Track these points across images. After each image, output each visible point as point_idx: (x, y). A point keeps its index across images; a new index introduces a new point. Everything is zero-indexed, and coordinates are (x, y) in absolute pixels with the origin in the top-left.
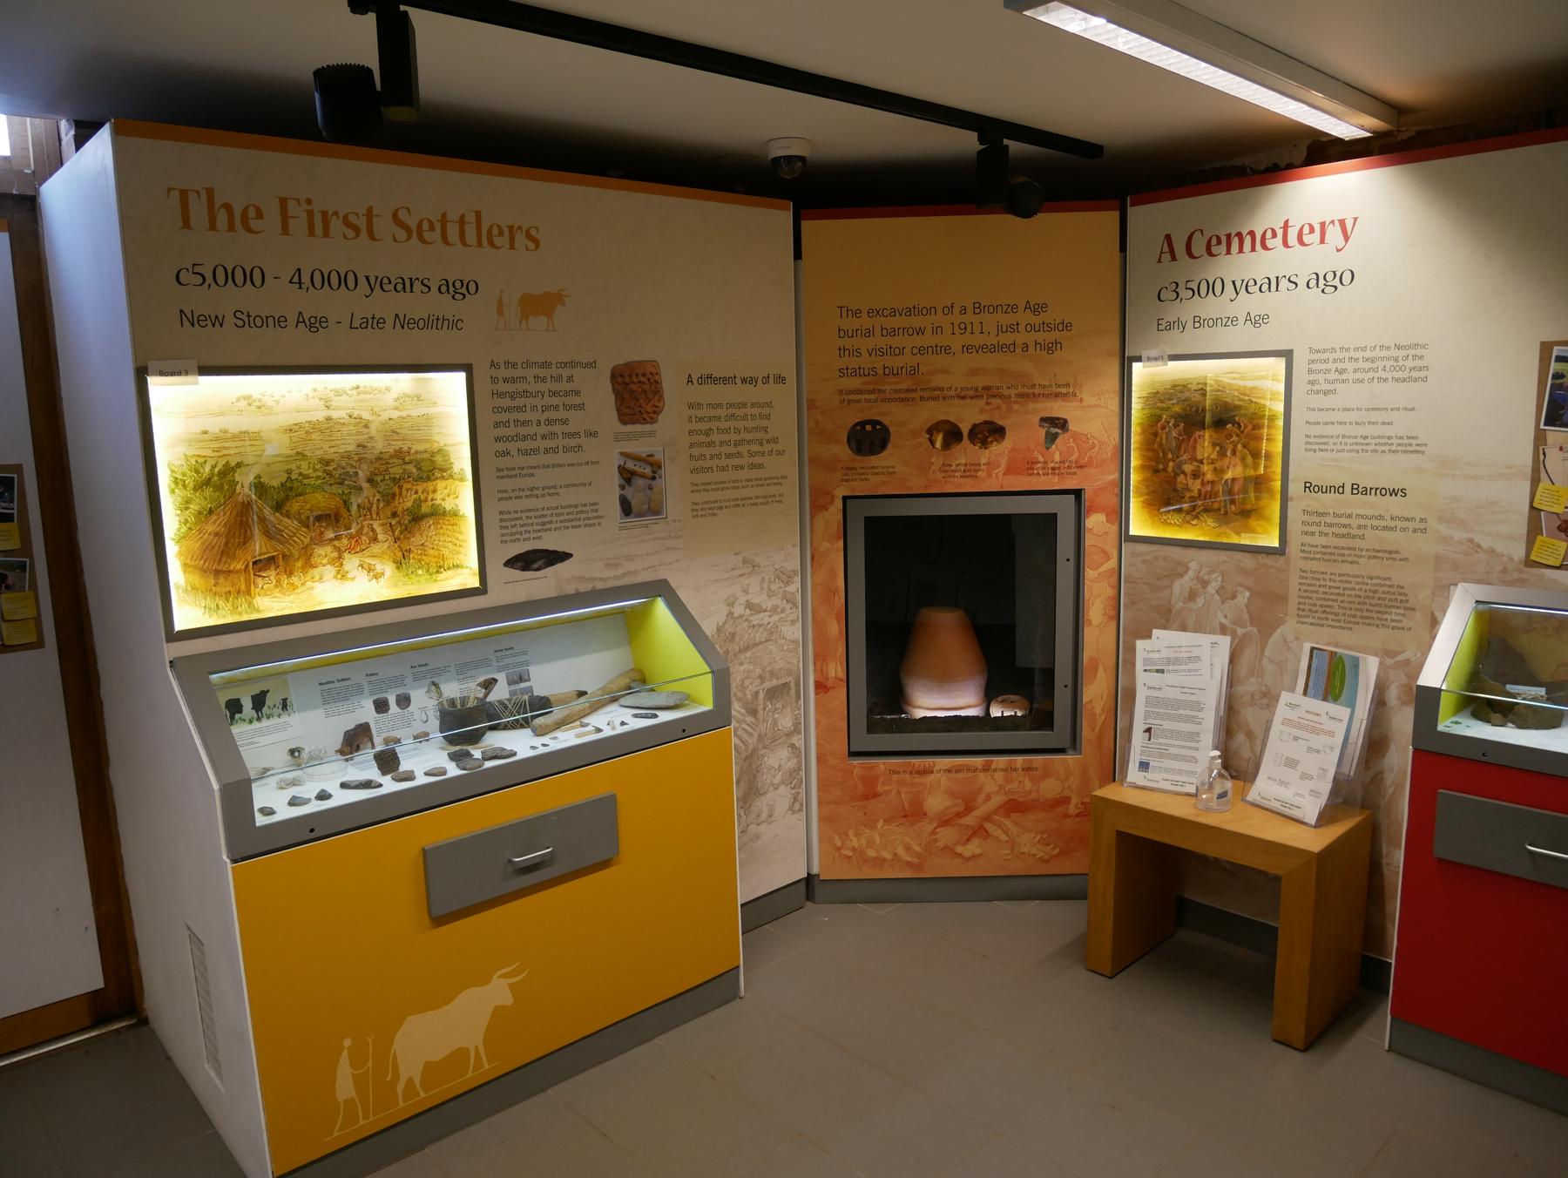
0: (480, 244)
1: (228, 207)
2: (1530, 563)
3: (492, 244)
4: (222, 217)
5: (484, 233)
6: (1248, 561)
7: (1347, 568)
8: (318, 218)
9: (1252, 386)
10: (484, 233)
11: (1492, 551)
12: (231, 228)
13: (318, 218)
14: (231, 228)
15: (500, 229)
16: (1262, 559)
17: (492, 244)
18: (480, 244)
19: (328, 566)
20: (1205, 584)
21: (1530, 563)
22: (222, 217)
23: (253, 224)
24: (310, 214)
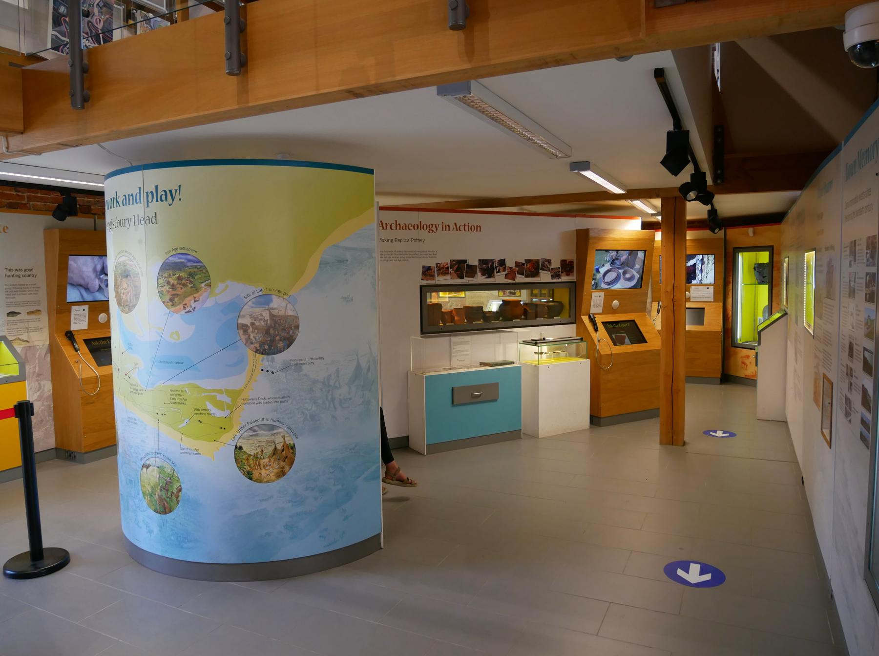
0: (469, 231)
1: (399, 224)
2: (499, 296)
3: (409, 229)
4: (398, 226)
5: (422, 226)
6: (459, 299)
7: (474, 299)
8: (444, 226)
9: (693, 264)
10: (422, 226)
11: (494, 295)
12: (400, 229)
13: (444, 226)
14: (400, 229)
15: (411, 226)
16: (462, 299)
17: (409, 229)
18: (469, 231)
19: (584, 366)
20: (453, 304)
21: (499, 296)
22: (398, 226)
23: (6, 231)
24: (443, 225)
